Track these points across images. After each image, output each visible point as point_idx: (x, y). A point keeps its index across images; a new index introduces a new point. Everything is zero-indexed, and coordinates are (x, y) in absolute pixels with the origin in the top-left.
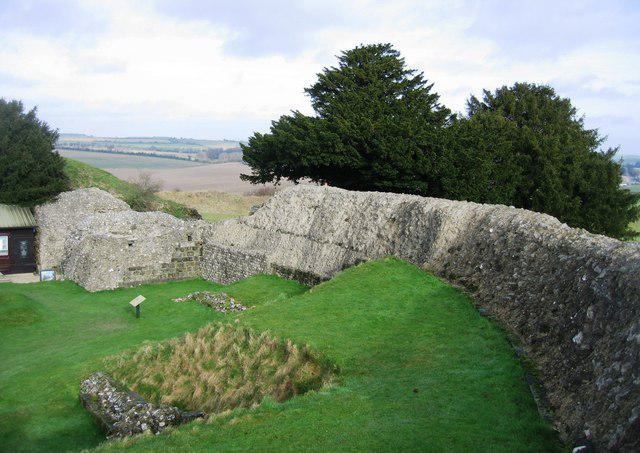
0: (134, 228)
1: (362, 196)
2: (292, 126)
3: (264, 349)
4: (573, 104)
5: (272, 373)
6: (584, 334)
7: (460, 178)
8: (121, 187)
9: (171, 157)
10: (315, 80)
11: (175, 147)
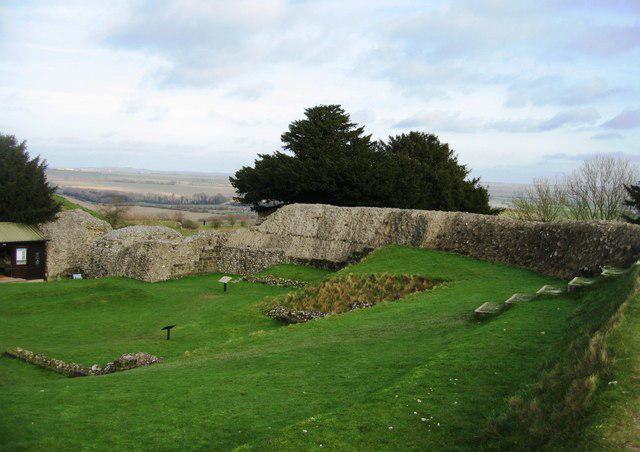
1: (355, 210)
2: (268, 163)
4: (450, 148)
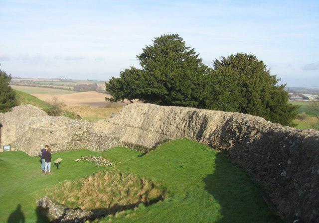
0: (51, 124)
1: (167, 108)
2: (130, 74)
3: (131, 182)
4: (265, 63)
5: (136, 194)
6: (287, 172)
7: (214, 99)
8: (42, 104)
9: (60, 88)
10: (142, 52)
11: (63, 83)
